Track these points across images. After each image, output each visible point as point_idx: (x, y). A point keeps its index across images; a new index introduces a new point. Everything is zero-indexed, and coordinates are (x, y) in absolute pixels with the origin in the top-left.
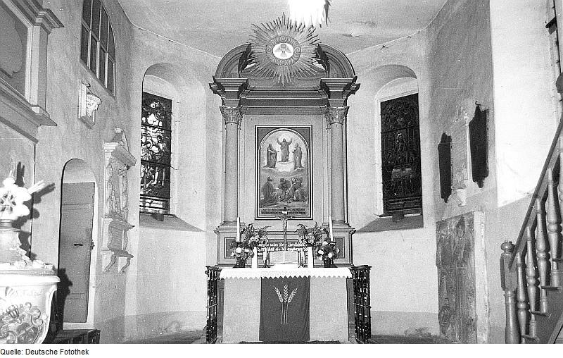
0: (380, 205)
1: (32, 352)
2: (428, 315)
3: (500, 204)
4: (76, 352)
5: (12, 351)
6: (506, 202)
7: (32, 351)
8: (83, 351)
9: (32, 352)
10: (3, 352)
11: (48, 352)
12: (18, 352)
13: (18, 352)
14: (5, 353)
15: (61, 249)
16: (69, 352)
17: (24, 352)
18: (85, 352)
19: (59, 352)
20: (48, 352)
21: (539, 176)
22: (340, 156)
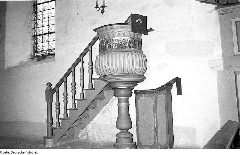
0: (235, 92)
1: (14, 152)
2: (40, 123)
3: (6, 68)
4: (33, 152)
5: (5, 152)
6: (8, 67)
7: (14, 152)
8: (35, 152)
9: (14, 152)
10: (1, 152)
11: (20, 153)
12: (8, 153)
13: (8, 153)
14: (2, 153)
15: (237, 27)
16: (29, 152)
17: (10, 153)
18: (36, 153)
19: (25, 152)
20: (20, 153)
21: (238, 93)
22: (116, 29)
